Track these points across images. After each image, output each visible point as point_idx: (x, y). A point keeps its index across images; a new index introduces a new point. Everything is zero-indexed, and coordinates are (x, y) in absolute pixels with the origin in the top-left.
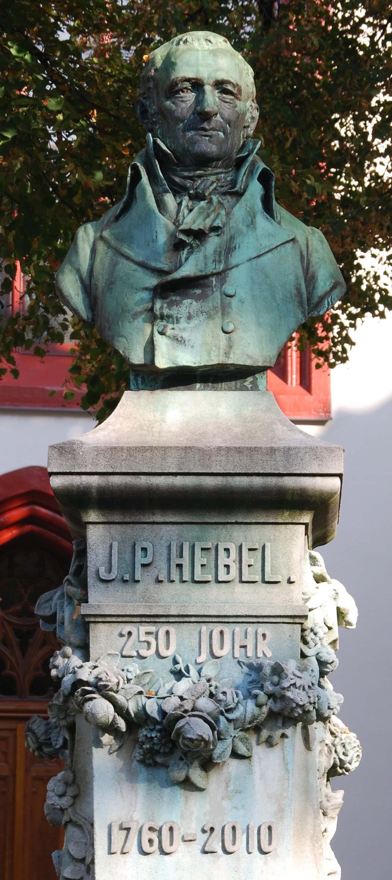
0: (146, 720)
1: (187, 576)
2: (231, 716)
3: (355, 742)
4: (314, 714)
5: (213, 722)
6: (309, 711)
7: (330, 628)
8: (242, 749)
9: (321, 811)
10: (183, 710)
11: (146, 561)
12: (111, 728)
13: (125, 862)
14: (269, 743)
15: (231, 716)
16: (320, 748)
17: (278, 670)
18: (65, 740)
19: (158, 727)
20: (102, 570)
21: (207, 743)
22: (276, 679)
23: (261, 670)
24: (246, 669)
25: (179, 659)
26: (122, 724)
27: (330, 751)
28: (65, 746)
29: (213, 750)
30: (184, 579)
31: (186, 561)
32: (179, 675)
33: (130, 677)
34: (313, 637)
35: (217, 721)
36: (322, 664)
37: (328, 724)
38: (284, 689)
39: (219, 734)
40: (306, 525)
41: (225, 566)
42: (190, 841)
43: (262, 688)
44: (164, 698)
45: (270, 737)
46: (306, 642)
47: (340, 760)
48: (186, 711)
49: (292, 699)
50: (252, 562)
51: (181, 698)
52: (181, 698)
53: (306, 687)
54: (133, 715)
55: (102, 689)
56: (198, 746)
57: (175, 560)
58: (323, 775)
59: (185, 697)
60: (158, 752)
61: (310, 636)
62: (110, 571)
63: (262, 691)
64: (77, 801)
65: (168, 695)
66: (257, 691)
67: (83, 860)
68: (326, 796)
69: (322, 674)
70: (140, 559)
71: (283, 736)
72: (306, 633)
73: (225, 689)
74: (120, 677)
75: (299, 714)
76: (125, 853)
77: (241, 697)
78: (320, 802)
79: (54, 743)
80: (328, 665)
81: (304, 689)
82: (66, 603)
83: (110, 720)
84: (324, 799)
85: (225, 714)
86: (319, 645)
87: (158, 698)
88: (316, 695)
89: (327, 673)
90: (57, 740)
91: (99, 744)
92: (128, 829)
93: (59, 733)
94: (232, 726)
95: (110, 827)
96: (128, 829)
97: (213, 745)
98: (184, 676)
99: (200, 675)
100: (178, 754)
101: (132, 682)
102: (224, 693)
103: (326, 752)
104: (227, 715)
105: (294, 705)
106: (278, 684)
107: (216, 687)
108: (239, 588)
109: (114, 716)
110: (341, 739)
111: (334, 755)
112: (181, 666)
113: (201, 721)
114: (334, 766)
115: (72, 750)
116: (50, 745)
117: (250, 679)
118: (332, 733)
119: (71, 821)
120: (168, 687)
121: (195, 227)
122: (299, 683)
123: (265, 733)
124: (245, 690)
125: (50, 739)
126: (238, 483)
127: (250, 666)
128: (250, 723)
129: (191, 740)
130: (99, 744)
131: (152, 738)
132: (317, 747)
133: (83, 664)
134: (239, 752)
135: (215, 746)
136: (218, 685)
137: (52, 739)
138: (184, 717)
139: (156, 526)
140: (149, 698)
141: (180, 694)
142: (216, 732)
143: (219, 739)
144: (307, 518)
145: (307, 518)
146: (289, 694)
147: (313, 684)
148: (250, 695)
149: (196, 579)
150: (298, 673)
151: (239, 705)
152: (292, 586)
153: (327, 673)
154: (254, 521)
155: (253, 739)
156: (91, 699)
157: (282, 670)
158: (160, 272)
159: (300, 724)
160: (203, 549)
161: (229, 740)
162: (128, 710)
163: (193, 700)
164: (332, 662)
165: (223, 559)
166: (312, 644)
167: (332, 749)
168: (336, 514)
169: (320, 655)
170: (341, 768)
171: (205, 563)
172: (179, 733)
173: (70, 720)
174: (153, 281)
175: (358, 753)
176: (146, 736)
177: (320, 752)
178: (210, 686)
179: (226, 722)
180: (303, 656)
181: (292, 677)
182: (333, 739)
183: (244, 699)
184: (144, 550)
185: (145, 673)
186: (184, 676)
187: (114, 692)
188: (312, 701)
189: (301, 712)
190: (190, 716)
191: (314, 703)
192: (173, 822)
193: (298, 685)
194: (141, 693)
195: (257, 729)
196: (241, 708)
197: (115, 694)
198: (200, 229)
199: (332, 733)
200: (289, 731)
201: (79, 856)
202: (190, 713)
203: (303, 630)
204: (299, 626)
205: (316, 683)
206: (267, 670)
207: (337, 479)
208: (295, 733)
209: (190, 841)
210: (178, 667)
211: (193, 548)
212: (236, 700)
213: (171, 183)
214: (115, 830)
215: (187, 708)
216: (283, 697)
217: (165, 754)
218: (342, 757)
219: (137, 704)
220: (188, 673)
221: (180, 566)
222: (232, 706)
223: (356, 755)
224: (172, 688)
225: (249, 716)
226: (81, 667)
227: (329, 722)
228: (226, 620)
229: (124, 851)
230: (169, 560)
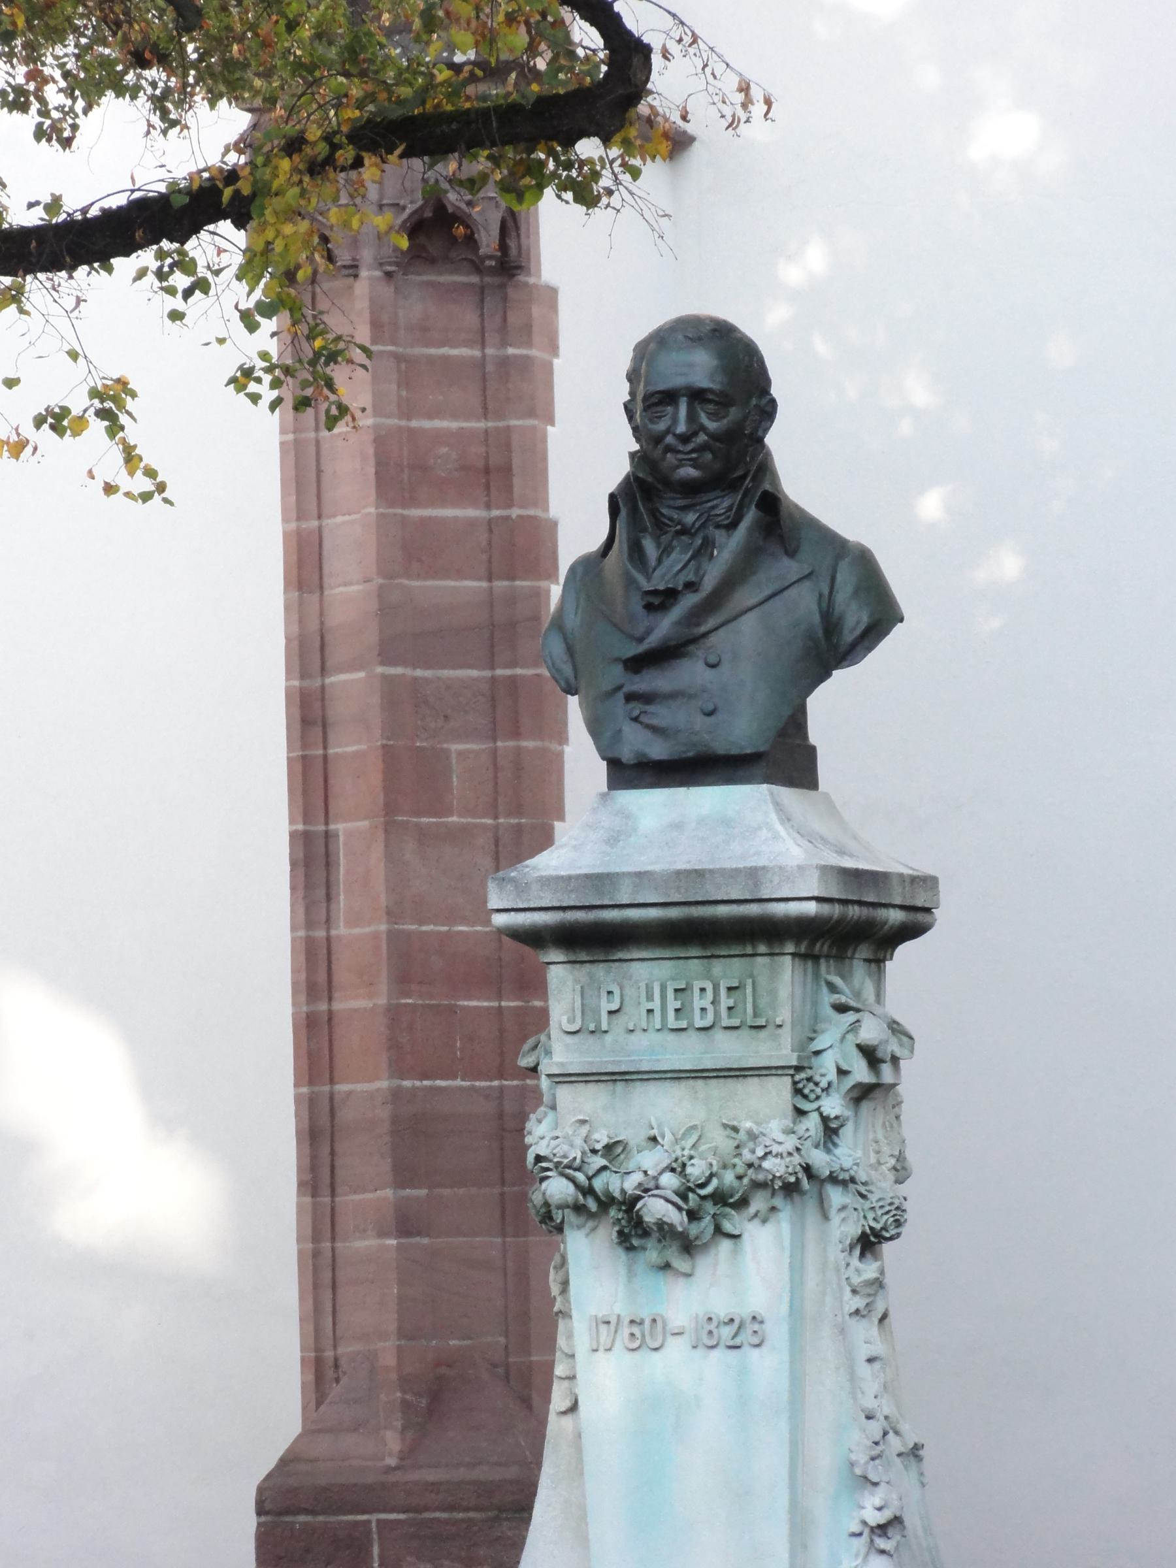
2: (703, 1192)
9: (848, 1289)
15: (703, 1192)
20: (564, 1019)
31: (656, 1005)
47: (871, 1228)
48: (646, 1191)
96: (608, 1323)
112: (655, 1132)
113: (662, 1201)
121: (661, 587)
156: (547, 1177)
161: (707, 1220)
166: (812, 1096)
193: (774, 1153)
213: (655, 514)
220: (663, 1138)
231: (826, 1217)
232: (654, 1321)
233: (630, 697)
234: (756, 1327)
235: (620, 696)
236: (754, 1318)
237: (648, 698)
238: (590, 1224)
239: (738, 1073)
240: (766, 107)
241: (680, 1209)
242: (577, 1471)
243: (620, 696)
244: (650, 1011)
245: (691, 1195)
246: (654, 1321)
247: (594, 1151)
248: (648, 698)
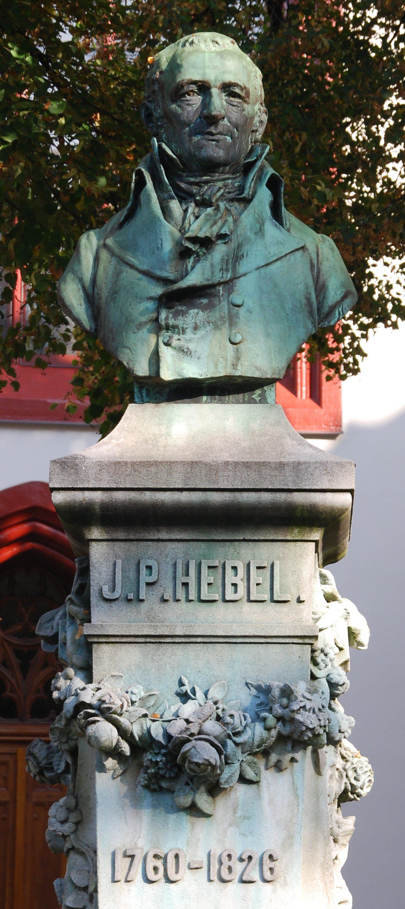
0: (151, 744)
1: (193, 595)
2: (238, 740)
3: (366, 766)
4: (324, 737)
5: (220, 745)
6: (319, 735)
7: (341, 649)
8: (250, 774)
9: (332, 838)
10: (189, 733)
11: (151, 580)
12: (114, 752)
13: (129, 890)
14: (278, 767)
15: (238, 740)
16: (330, 773)
17: (287, 693)
18: (67, 764)
19: (163, 751)
20: (106, 589)
21: (214, 767)
22: (285, 701)
23: (270, 692)
24: (254, 691)
25: (185, 681)
26: (126, 748)
27: (341, 776)
28: (67, 770)
29: (220, 775)
30: (190, 598)
33: (134, 699)
34: (324, 658)
35: (224, 744)
36: (333, 685)
37: (339, 748)
38: (293, 711)
39: (226, 758)
40: (316, 542)
41: (233, 584)
42: (197, 868)
43: (270, 711)
44: (169, 721)
45: (279, 761)
46: (316, 664)
47: (352, 785)
48: (192, 735)
49: (302, 722)
50: (260, 581)
51: (187, 721)
52: (187, 721)
53: (317, 710)
54: (137, 739)
55: (105, 712)
56: (205, 770)
57: (181, 579)
58: (334, 801)
59: (191, 720)
60: (163, 777)
61: (320, 657)
62: (113, 589)
63: (271, 713)
64: (80, 827)
65: (174, 718)
66: (265, 714)
67: (85, 889)
68: (337, 822)
70: (144, 577)
71: (293, 760)
72: (317, 654)
73: (233, 712)
74: (124, 700)
75: (309, 738)
76: (129, 881)
77: (249, 720)
78: (331, 829)
79: (55, 768)
80: (339, 687)
81: (314, 712)
82: (68, 623)
83: (114, 744)
84: (335, 826)
85: (233, 737)
86: (329, 667)
87: (163, 721)
88: (326, 718)
89: (338, 695)
90: (59, 765)
91: (102, 769)
92: (132, 857)
93: (61, 757)
94: (239, 750)
95: (114, 855)
96: (132, 857)
97: (220, 770)
98: (190, 698)
99: (206, 697)
100: (184, 779)
101: (136, 704)
102: (232, 716)
103: (337, 777)
104: (235, 739)
105: (304, 728)
106: (287, 707)
107: (223, 710)
109: (118, 740)
110: (352, 764)
111: (345, 780)
112: (187, 688)
113: (207, 745)
114: (345, 791)
115: (75, 775)
116: (51, 769)
117: (258, 701)
118: (343, 758)
119: (73, 848)
120: (173, 709)
121: (201, 235)
122: (309, 705)
123: (274, 758)
124: (253, 713)
125: (51, 763)
126: (245, 499)
127: (258, 688)
128: (258, 747)
129: (197, 764)
130: (102, 769)
131: (157, 762)
132: (327, 772)
133: (86, 686)
134: (247, 777)
135: (222, 771)
136: (225, 707)
137: (54, 764)
138: (190, 741)
139: (161, 544)
140: (154, 721)
141: (186, 717)
142: (223, 757)
143: (227, 763)
144: (317, 535)
145: (317, 535)
146: (298, 717)
147: (323, 707)
149: (203, 598)
150: (308, 695)
151: (247, 728)
152: (301, 605)
153: (338, 695)
154: (262, 538)
155: (261, 763)
156: (94, 722)
157: (292, 692)
158: (166, 281)
159: (310, 748)
160: (209, 567)
161: (237, 765)
162: (132, 733)
163: (200, 723)
164: (343, 684)
165: (230, 578)
166: (322, 665)
168: (347, 531)
169: (331, 676)
170: (352, 793)
171: (212, 582)
172: (185, 757)
173: (72, 743)
175: (370, 778)
176: (151, 760)
177: (331, 777)
178: (217, 708)
179: (234, 746)
180: (313, 677)
181: (302, 699)
182: (345, 763)
183: (252, 722)
184: (149, 568)
185: (150, 695)
186: (190, 698)
187: (118, 715)
188: (323, 724)
189: (311, 735)
190: (196, 739)
191: (325, 726)
192: (179, 849)
193: (308, 707)
194: (145, 716)
195: (266, 753)
196: (249, 731)
197: (118, 717)
198: (206, 237)
199: (343, 758)
201: (81, 884)
202: (196, 737)
203: (313, 651)
204: (309, 647)
205: (327, 705)
206: (276, 692)
207: (349, 495)
208: (304, 758)
209: (197, 868)
210: (184, 689)
212: (244, 723)
213: (177, 189)
214: (119, 857)
215: (193, 731)
217: (171, 779)
218: (354, 782)
219: (142, 727)
220: (194, 694)
221: (186, 585)
222: (240, 729)
223: (367, 780)
224: (177, 711)
225: (257, 740)
226: (84, 689)
227: (340, 746)
228: (234, 640)
229: (128, 879)
230: (175, 578)
232: (177, 856)
234: (272, 865)
236: (271, 857)
239: (183, 640)
241: (220, 752)
245: (229, 742)
246: (177, 856)
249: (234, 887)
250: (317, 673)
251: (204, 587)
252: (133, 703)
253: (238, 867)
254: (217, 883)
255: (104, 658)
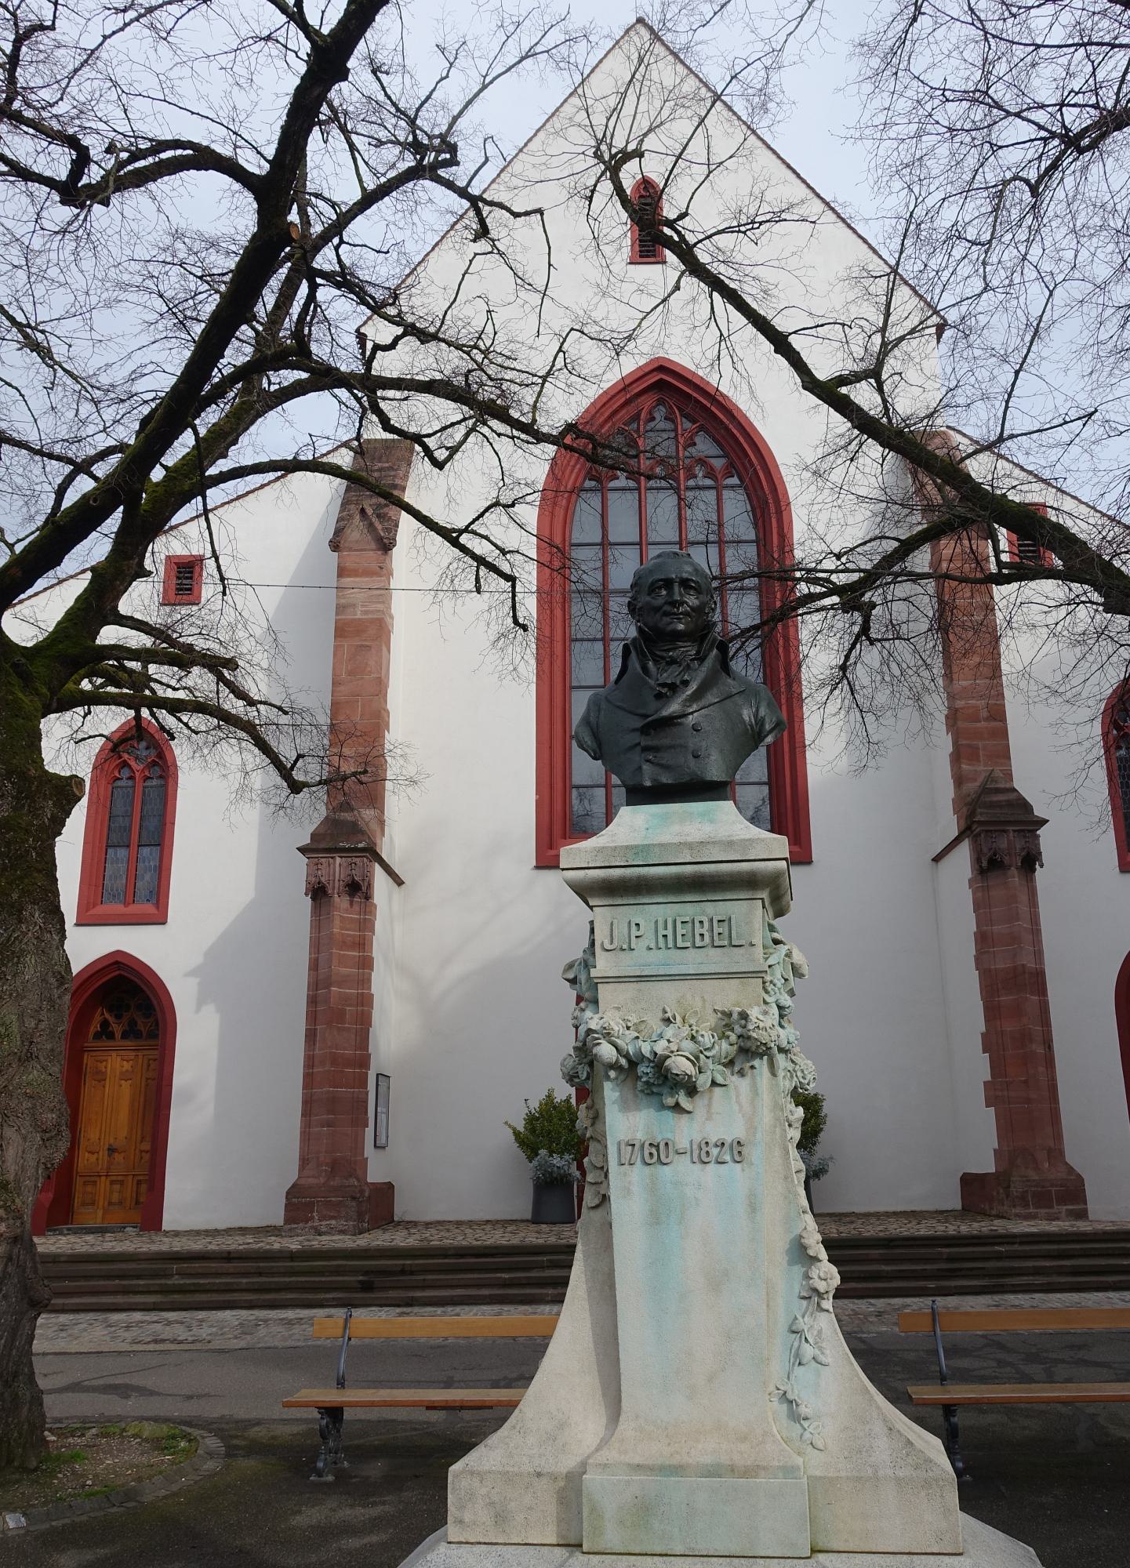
1: (671, 944)
8: (720, 1080)
17: (744, 1016)
21: (690, 1077)
26: (623, 1061)
28: (588, 1078)
31: (669, 932)
32: (668, 1021)
35: (697, 1058)
36: (780, 1008)
43: (732, 1030)
46: (767, 992)
55: (607, 1035)
57: (662, 932)
61: (770, 988)
69: (781, 1016)
70: (634, 932)
91: (608, 1078)
95: (619, 1143)
106: (744, 1027)
108: (712, 952)
112: (669, 1015)
122: (761, 1025)
123: (736, 1069)
127: (723, 1013)
130: (608, 1078)
132: (781, 1073)
144: (765, 894)
145: (765, 894)
146: (754, 1035)
148: (723, 1036)
155: (727, 1071)
165: (698, 931)
167: (792, 1073)
172: (668, 1070)
174: (639, 723)
180: (765, 1002)
200: (756, 1063)
205: (776, 1023)
206: (735, 1016)
208: (761, 1064)
211: (675, 921)
213: (652, 654)
214: (623, 1146)
216: (749, 1038)
221: (665, 936)
231: (774, 1074)
233: (646, 749)
235: (638, 749)
237: (655, 749)
238: (622, 1077)
240: (521, 621)
242: (607, 1246)
243: (638, 749)
244: (665, 936)
247: (628, 1028)
248: (655, 749)
249: (712, 1166)
250: (768, 999)
251: (679, 938)
252: (628, 1028)
253: (715, 1151)
254: (698, 1166)
255: (604, 992)
